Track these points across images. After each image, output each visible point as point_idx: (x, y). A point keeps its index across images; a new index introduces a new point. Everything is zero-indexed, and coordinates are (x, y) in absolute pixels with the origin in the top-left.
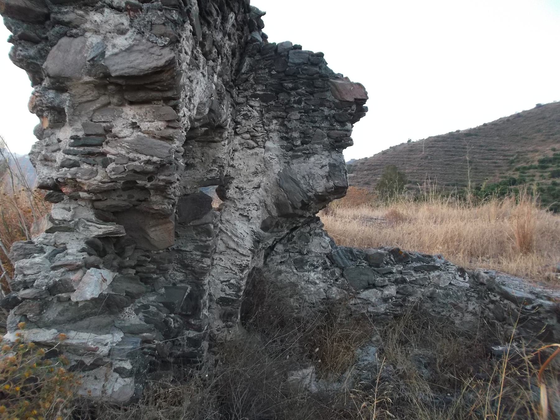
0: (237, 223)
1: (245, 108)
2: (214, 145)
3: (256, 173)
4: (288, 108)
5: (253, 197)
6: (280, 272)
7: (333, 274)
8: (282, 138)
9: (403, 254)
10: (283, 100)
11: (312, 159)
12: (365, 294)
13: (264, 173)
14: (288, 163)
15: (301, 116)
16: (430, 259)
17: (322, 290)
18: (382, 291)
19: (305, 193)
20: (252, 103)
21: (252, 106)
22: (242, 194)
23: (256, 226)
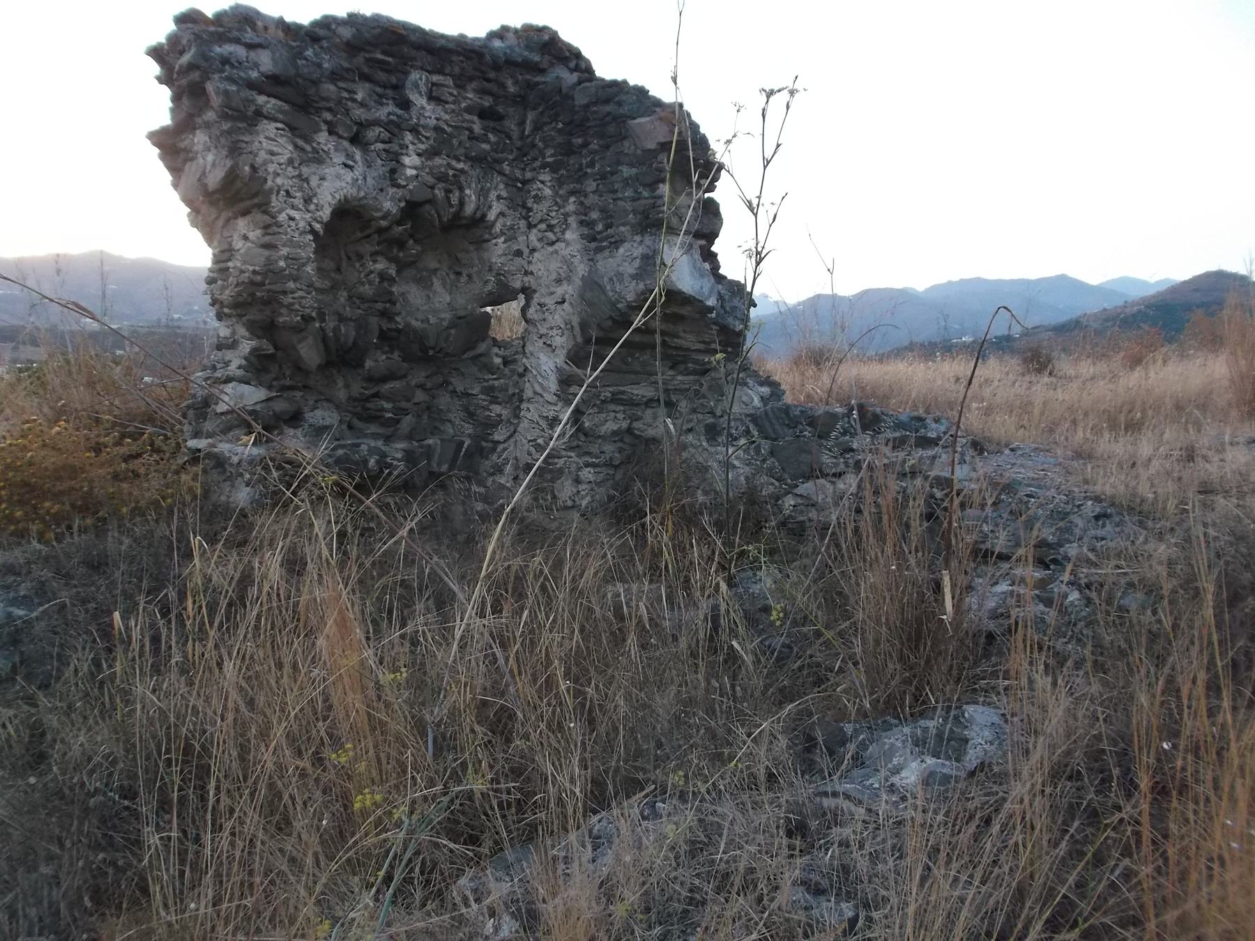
0: (542, 356)
1: (535, 187)
2: (485, 245)
3: (559, 281)
4: (581, 177)
5: (556, 317)
6: (684, 447)
7: (758, 450)
8: (581, 223)
9: (869, 415)
10: (573, 165)
11: (621, 250)
12: (806, 488)
13: (569, 279)
14: (591, 260)
15: (598, 185)
16: (920, 423)
17: (742, 478)
18: (833, 483)
19: (614, 304)
20: (542, 177)
21: (542, 182)
22: (544, 313)
23: (560, 359)
